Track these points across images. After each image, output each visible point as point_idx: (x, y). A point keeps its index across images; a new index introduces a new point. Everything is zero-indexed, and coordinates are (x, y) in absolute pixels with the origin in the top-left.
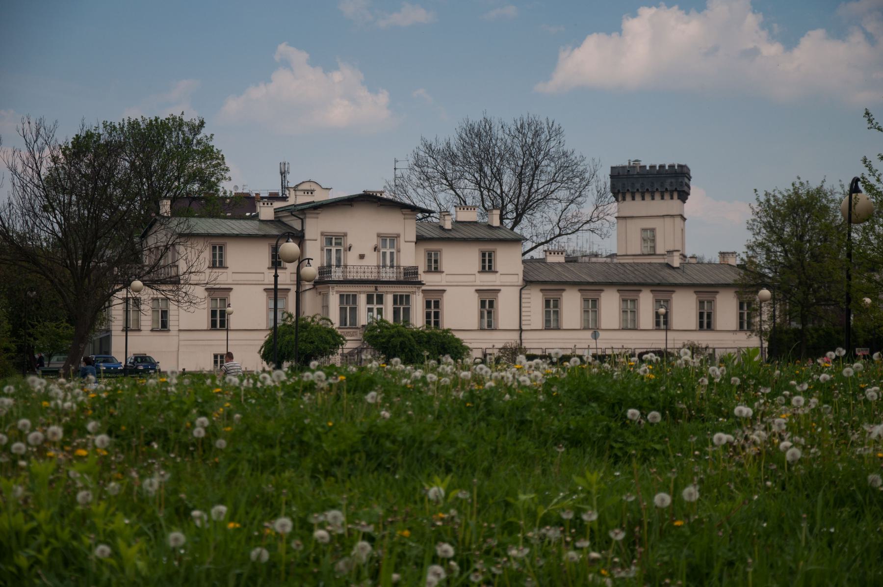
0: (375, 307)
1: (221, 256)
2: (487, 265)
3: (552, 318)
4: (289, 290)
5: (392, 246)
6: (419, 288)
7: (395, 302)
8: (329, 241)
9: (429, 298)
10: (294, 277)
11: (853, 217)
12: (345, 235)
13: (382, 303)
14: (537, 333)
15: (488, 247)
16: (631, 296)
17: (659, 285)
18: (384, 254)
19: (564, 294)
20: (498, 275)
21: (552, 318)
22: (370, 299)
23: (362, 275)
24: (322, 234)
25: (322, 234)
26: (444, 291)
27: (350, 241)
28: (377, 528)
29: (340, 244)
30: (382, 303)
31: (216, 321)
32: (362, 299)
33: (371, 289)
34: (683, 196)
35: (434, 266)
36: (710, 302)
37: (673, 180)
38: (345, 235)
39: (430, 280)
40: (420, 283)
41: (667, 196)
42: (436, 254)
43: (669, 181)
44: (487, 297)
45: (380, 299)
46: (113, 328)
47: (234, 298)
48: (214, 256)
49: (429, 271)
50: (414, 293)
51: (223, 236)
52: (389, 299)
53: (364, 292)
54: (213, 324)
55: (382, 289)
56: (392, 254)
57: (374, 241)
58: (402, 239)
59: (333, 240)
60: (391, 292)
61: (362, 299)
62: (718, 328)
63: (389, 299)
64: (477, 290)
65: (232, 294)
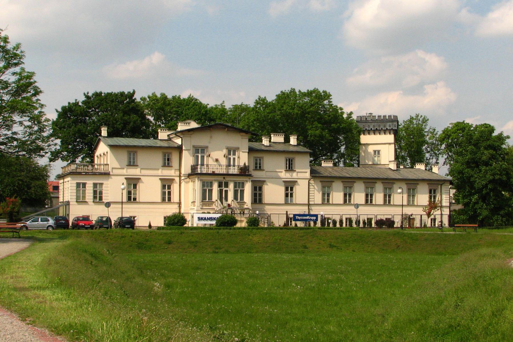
1: (134, 159)
3: (326, 201)
6: (250, 178)
7: (235, 186)
9: (288, 184)
11: (259, 155)
12: (207, 147)
13: (227, 187)
15: (290, 156)
16: (412, 186)
17: (386, 179)
18: (230, 159)
20: (264, 172)
21: (326, 201)
22: (220, 185)
23: (216, 170)
24: (194, 146)
25: (194, 146)
26: (264, 181)
30: (227, 187)
31: (346, 199)
33: (221, 178)
35: (258, 167)
36: (414, 190)
37: (391, 124)
39: (257, 175)
40: (250, 175)
42: (260, 160)
43: (388, 124)
45: (227, 185)
47: (141, 186)
48: (130, 158)
49: (256, 169)
50: (247, 181)
51: (135, 147)
52: (231, 186)
53: (233, 181)
54: (164, 199)
55: (228, 179)
56: (234, 159)
57: (225, 151)
60: (233, 181)
62: (266, 202)
63: (231, 186)
64: (126, 178)
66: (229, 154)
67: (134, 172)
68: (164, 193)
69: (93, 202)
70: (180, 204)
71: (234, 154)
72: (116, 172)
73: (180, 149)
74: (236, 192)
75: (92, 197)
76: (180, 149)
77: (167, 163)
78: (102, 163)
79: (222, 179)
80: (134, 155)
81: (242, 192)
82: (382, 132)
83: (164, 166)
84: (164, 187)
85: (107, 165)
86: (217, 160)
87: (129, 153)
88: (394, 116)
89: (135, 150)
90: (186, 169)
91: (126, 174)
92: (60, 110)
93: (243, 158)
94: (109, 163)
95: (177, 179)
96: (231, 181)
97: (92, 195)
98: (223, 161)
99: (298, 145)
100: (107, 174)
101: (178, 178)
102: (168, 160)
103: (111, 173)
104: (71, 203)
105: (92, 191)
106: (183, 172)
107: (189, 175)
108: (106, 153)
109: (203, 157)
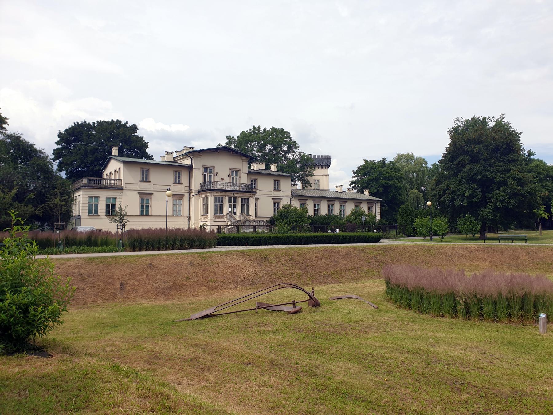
0: (232, 204)
1: (147, 175)
2: (277, 188)
4: (183, 195)
5: (236, 175)
7: (242, 202)
8: (205, 170)
10: (187, 189)
14: (136, 218)
18: (233, 178)
19: (335, 203)
22: (230, 201)
25: (203, 166)
27: (216, 170)
28: (36, 206)
29: (211, 172)
32: (226, 200)
33: (231, 194)
34: (328, 166)
38: (214, 168)
41: (324, 167)
43: (325, 161)
44: (277, 202)
45: (235, 201)
46: (100, 202)
48: (143, 175)
50: (251, 197)
52: (239, 200)
53: (227, 196)
55: (236, 195)
57: (229, 172)
58: (241, 172)
59: (207, 170)
60: (227, 196)
61: (226, 200)
63: (239, 200)
65: (152, 196)
66: (233, 175)
67: (146, 187)
68: (142, 206)
69: (88, 215)
70: (189, 217)
71: (236, 175)
72: (129, 187)
73: (190, 168)
74: (243, 206)
75: (105, 211)
76: (190, 168)
77: (178, 182)
78: (113, 178)
79: (232, 195)
80: (147, 171)
81: (248, 206)
82: (320, 167)
83: (142, 181)
84: (142, 200)
85: (120, 180)
86: (222, 179)
87: (175, 172)
88: (325, 156)
89: (179, 170)
90: (196, 185)
91: (139, 189)
92: (87, 123)
93: (244, 180)
94: (122, 178)
95: (187, 195)
96: (225, 196)
97: (105, 208)
98: (228, 180)
99: (278, 171)
100: (120, 189)
101: (188, 194)
102: (147, 175)
103: (124, 188)
104: (82, 217)
105: (105, 205)
106: (193, 187)
107: (199, 192)
108: (118, 170)
109: (210, 176)
